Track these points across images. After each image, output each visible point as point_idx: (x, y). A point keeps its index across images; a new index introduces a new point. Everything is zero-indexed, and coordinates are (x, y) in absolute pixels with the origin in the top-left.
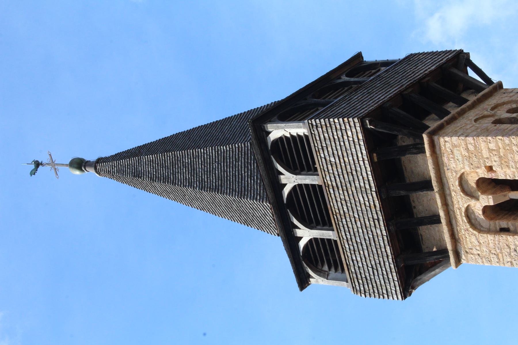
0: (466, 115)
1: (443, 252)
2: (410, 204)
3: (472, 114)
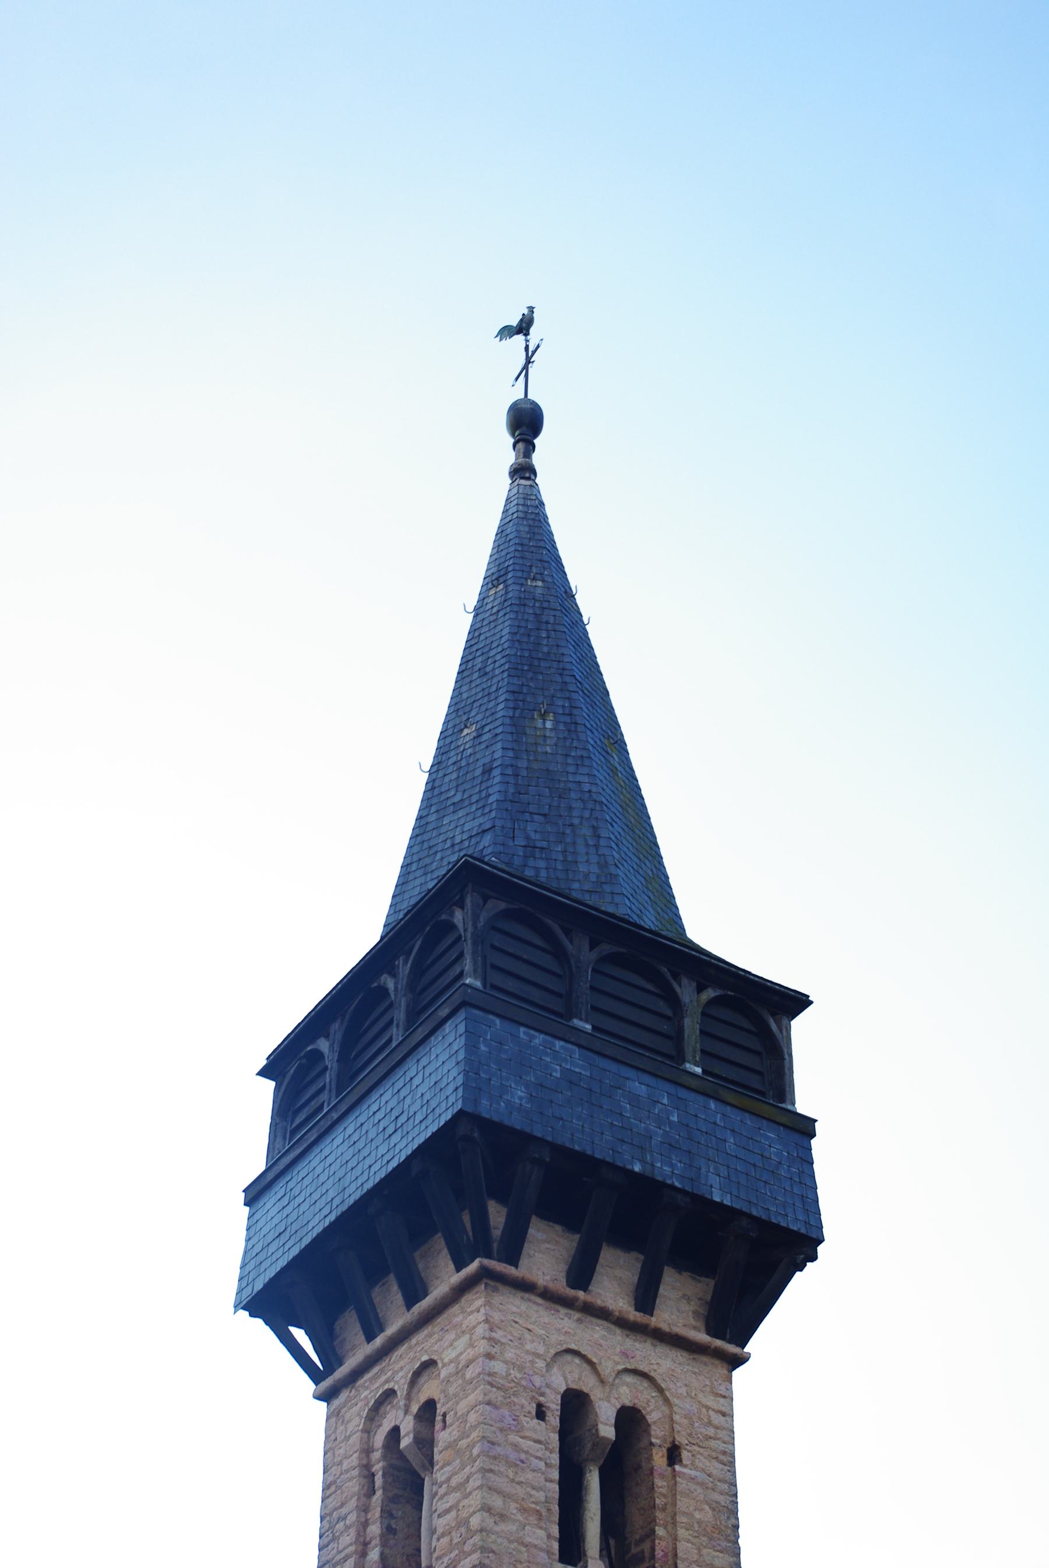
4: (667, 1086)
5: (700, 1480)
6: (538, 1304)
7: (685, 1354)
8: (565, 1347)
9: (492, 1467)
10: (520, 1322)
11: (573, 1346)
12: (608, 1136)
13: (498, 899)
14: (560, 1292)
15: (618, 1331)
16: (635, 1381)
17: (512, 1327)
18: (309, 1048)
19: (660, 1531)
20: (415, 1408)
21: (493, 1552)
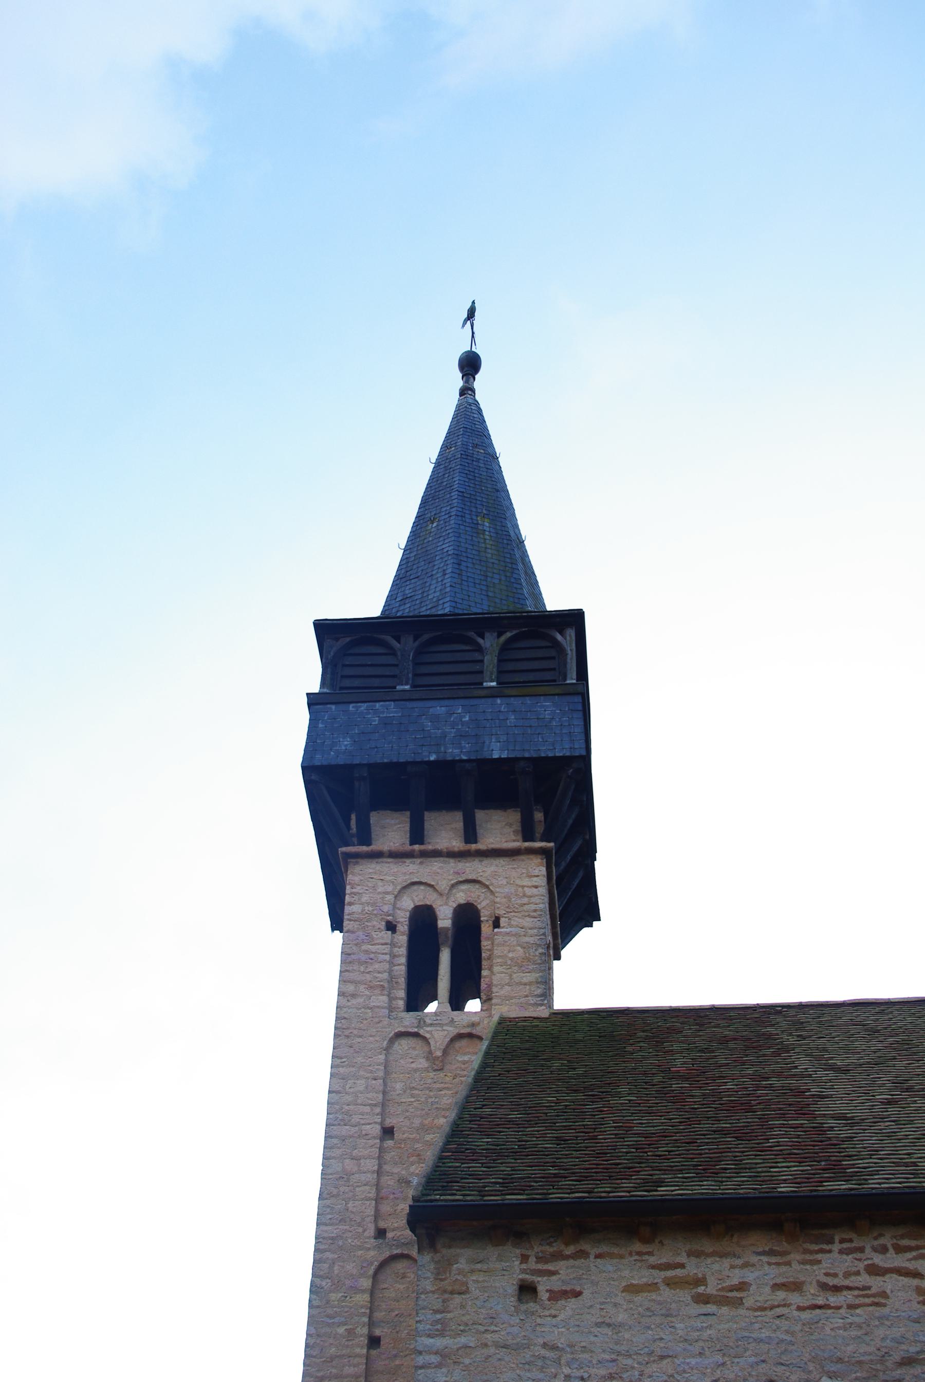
4: (457, 702)
5: (513, 933)
6: (389, 863)
7: (507, 859)
8: (409, 882)
9: (348, 969)
10: (375, 877)
11: (416, 880)
12: (411, 746)
13: (344, 637)
14: (400, 851)
15: (452, 860)
16: (469, 886)
17: (368, 881)
21: (345, 1018)
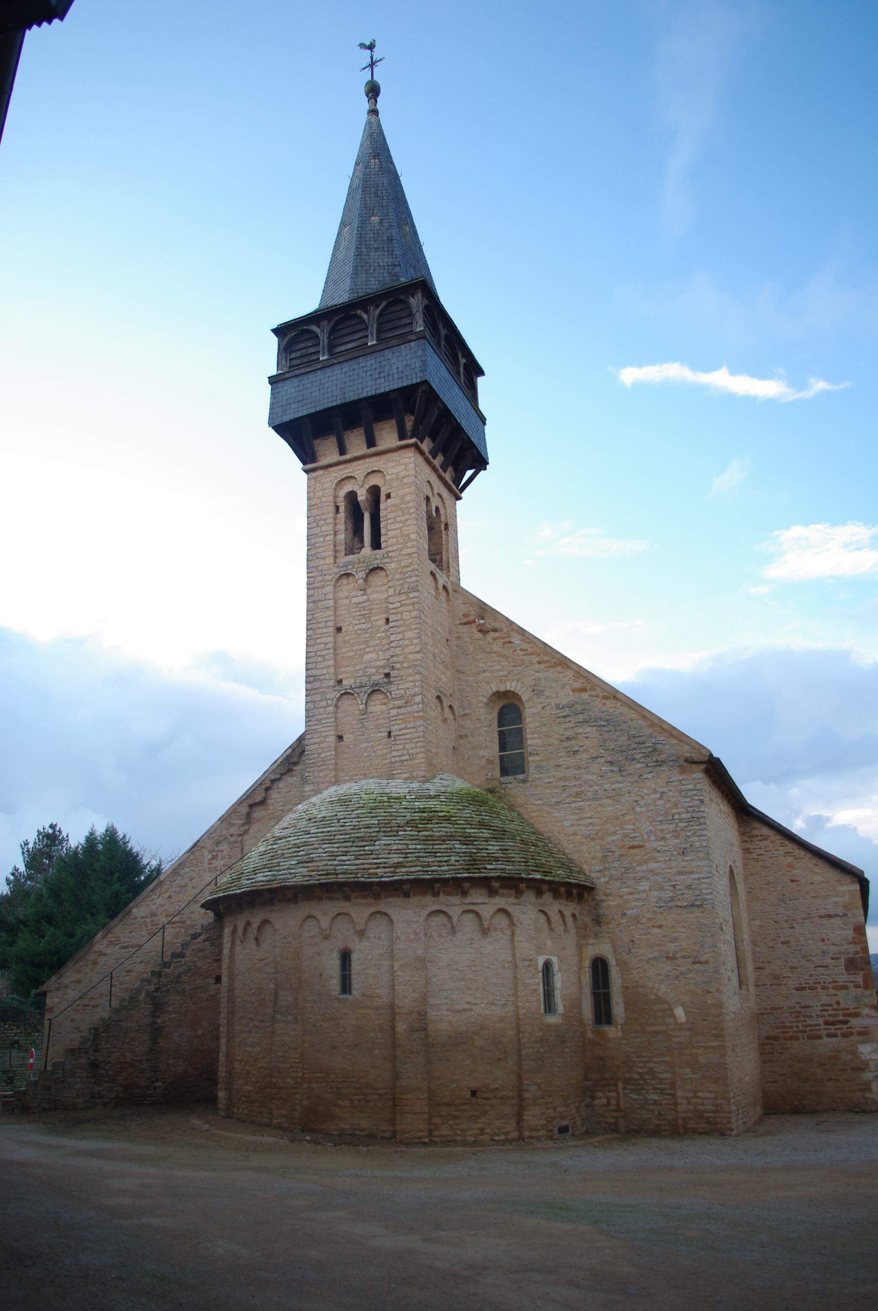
0: (433, 472)
1: (314, 459)
2: (355, 427)
3: (434, 479)
18: (305, 328)
19: (444, 553)
20: (367, 487)
